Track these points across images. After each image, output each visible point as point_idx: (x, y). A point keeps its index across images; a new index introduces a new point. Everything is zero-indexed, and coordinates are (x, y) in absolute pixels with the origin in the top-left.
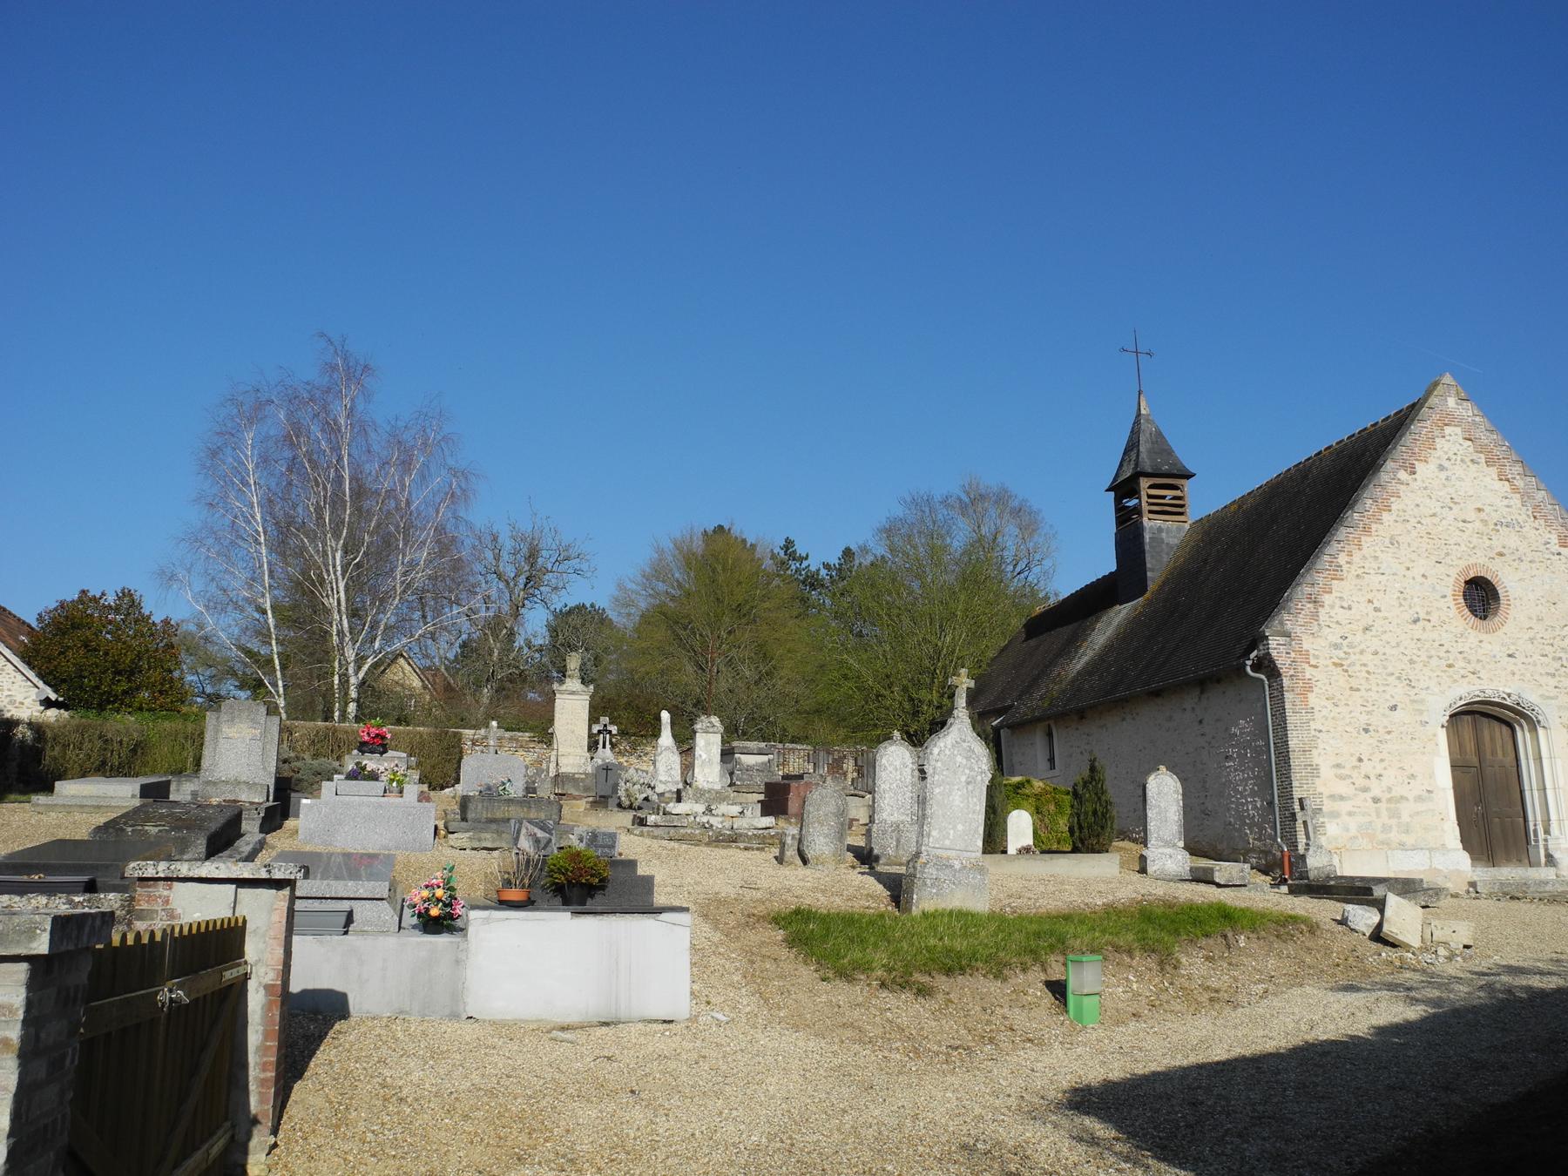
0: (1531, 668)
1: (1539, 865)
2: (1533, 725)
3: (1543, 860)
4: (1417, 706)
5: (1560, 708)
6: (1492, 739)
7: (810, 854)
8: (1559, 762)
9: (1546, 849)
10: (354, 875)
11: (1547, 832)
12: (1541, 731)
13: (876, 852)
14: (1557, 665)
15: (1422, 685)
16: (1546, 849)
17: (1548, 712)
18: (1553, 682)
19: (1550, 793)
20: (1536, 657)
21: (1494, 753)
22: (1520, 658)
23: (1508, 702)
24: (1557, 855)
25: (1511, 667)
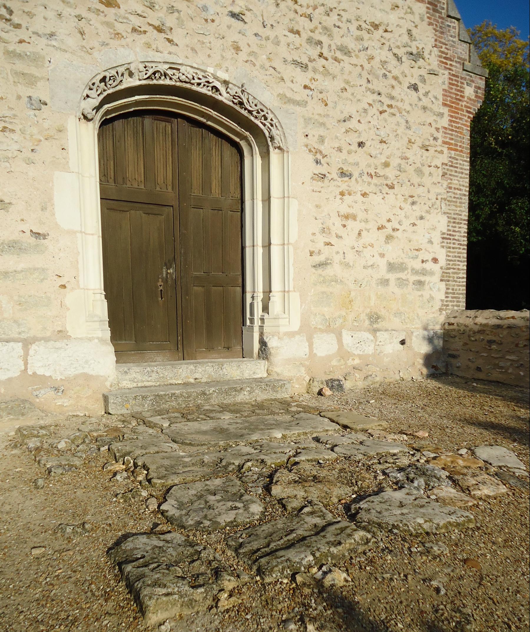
0: (270, 47)
1: (251, 356)
2: (264, 142)
3: (256, 346)
4: (20, 66)
5: (307, 121)
6: (206, 166)
7: (247, 64)
8: (294, 205)
9: (261, 334)
10: (203, 117)
11: (266, 309)
12: (274, 156)
13: (339, 44)
14: (314, 52)
15: (38, 24)
16: (261, 334)
17: (290, 127)
18: (302, 78)
19: (275, 250)
20: (281, 31)
21: (206, 185)
22: (253, 26)
23: (224, 98)
24: (272, 343)
25: (233, 36)
